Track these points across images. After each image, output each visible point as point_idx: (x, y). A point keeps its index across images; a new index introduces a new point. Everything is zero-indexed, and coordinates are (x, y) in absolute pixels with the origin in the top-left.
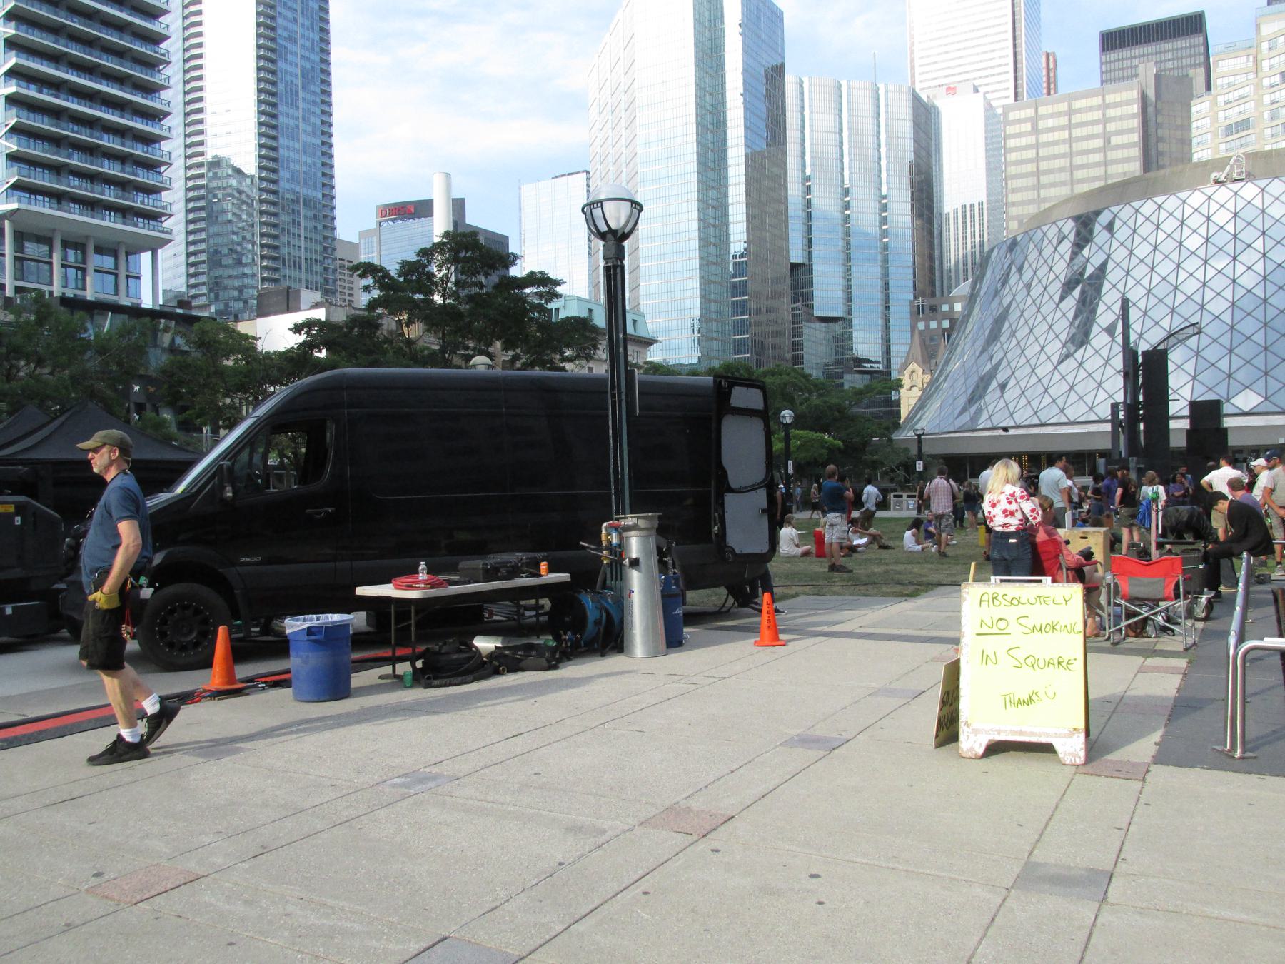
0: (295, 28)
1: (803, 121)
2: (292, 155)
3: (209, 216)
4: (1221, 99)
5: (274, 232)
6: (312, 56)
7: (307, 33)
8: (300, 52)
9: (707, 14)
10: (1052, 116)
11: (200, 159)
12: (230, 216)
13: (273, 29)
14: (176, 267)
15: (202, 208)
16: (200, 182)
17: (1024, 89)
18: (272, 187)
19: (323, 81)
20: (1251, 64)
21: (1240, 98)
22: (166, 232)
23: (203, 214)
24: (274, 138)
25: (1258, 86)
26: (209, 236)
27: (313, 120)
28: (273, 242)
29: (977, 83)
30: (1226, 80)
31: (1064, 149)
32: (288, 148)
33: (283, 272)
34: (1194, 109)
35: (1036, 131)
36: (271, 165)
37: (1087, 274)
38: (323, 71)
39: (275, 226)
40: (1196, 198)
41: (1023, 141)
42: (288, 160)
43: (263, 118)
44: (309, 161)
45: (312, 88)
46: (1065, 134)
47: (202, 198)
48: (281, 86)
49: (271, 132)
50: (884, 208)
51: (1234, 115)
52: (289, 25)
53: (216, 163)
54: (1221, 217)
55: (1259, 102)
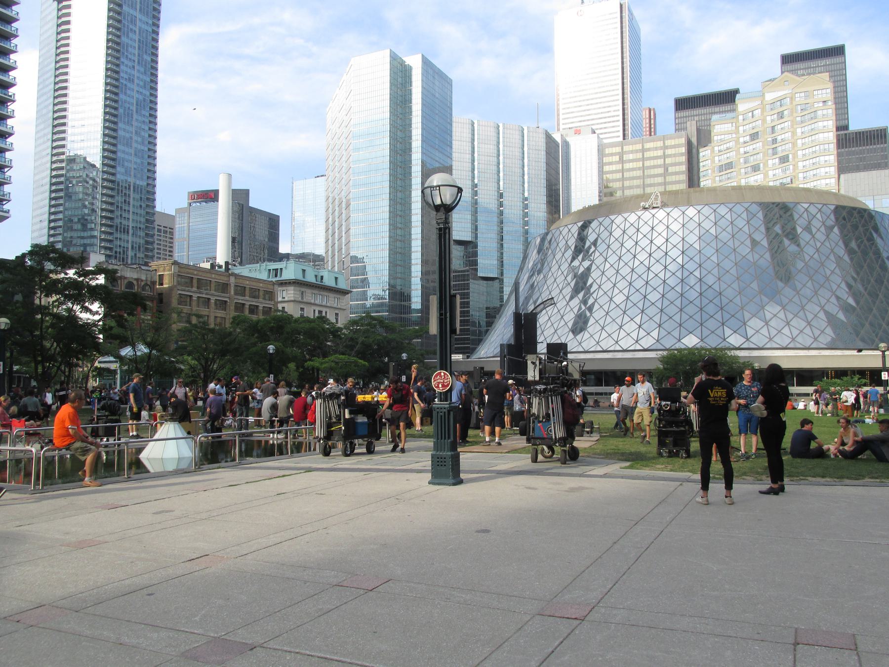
0: (133, 72)
1: (473, 148)
2: (126, 157)
3: (66, 195)
4: (716, 149)
5: (111, 208)
6: (144, 91)
7: (141, 76)
8: (136, 88)
9: (399, 80)
10: (632, 152)
11: (62, 157)
12: (81, 196)
13: (117, 72)
14: (41, 229)
15: (61, 190)
16: (60, 172)
17: (629, 132)
18: (111, 177)
19: (151, 108)
20: (734, 128)
21: (728, 149)
22: (5, 212)
23: (62, 194)
24: (114, 145)
25: (737, 142)
26: (65, 209)
27: (143, 133)
28: (109, 215)
29: (594, 127)
30: (719, 137)
31: (639, 173)
32: (124, 152)
33: (115, 235)
34: (701, 154)
35: (622, 161)
36: (112, 163)
37: (786, 242)
38: (151, 102)
39: (112, 204)
40: (632, 218)
41: (614, 167)
42: (123, 160)
43: (107, 132)
44: (139, 161)
45: (143, 112)
46: (640, 164)
47: (61, 183)
48: (121, 111)
49: (112, 141)
50: (526, 207)
51: (724, 159)
52: (129, 71)
53: (72, 160)
54: (675, 227)
55: (738, 152)
